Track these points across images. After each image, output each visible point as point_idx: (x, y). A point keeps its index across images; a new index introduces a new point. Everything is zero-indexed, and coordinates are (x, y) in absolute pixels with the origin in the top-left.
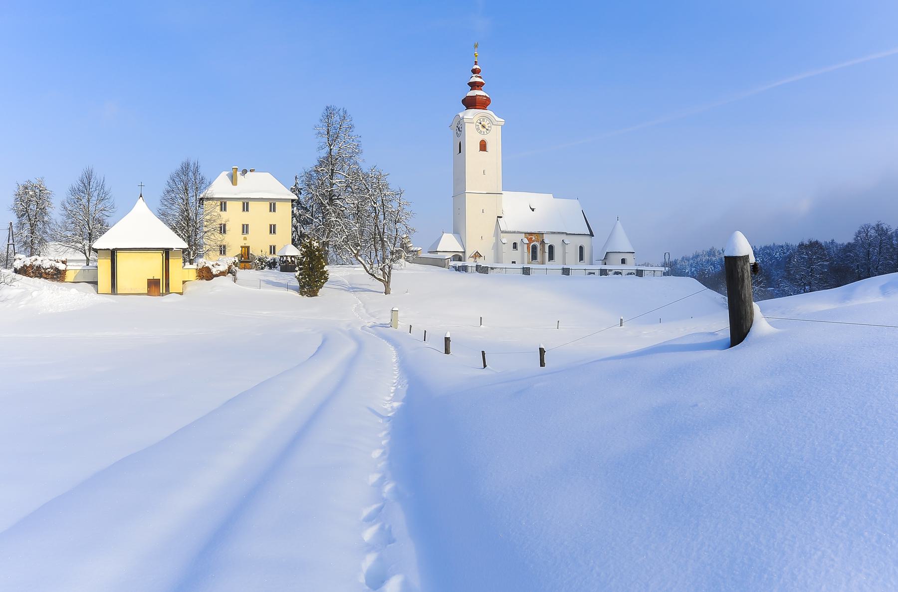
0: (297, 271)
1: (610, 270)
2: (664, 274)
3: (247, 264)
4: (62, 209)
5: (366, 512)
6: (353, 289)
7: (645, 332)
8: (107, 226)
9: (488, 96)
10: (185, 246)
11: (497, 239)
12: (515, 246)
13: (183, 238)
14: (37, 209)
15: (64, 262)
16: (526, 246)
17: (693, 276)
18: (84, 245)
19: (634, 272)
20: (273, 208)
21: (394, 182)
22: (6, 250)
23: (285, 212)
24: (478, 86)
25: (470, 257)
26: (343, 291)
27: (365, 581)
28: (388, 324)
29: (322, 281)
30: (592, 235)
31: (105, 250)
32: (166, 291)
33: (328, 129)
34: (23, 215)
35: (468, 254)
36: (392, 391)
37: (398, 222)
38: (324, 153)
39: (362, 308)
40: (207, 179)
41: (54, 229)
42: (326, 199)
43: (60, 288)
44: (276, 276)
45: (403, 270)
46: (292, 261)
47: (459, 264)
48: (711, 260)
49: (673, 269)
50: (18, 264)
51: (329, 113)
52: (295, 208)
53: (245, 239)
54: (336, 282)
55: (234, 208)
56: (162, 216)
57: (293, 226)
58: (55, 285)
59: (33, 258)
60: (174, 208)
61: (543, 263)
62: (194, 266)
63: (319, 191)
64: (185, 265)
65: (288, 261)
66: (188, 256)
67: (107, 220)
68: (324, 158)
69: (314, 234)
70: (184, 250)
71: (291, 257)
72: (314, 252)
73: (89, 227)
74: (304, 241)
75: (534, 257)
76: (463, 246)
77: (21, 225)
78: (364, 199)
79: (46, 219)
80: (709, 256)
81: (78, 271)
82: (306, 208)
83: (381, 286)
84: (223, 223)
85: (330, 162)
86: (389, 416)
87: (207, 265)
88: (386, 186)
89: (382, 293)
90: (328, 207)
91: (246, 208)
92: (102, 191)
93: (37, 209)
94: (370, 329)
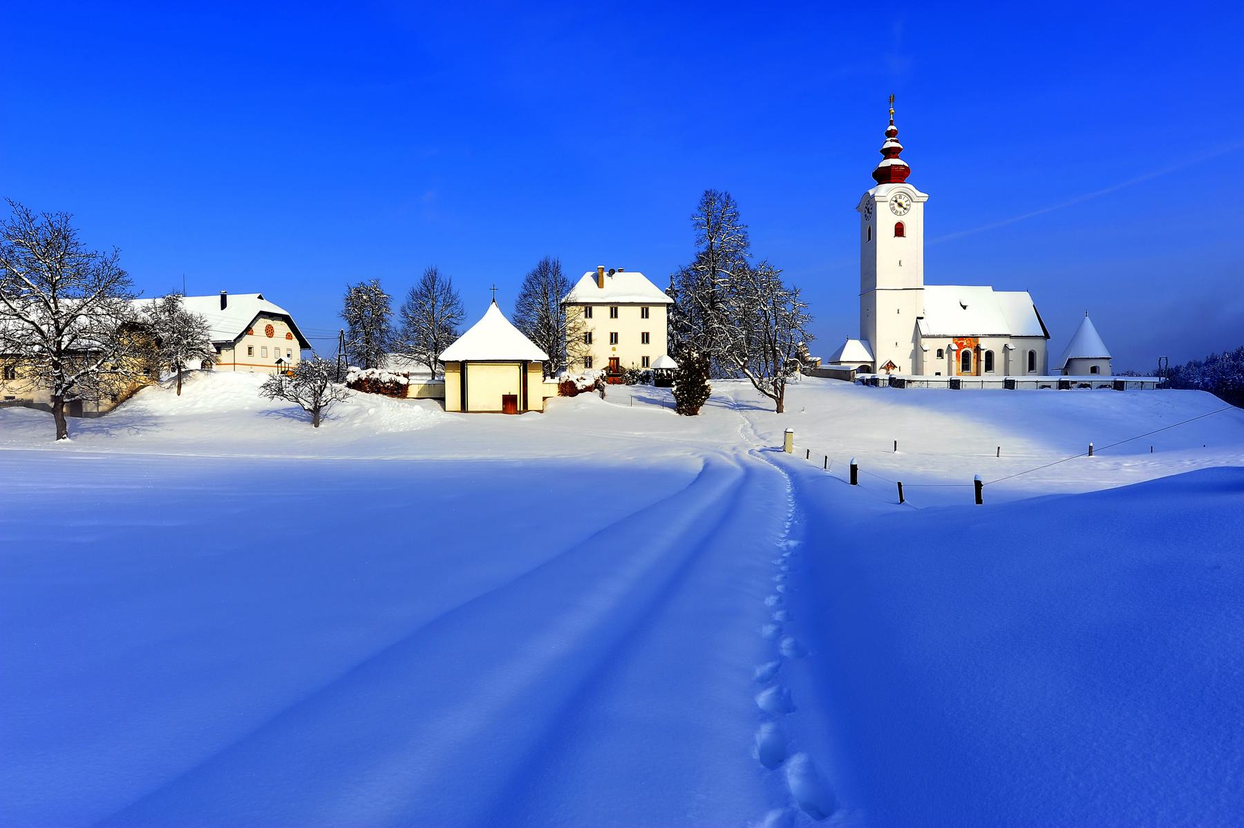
0: (673, 386)
1: (1073, 382)
2: (1159, 386)
3: (616, 378)
4: (402, 316)
5: (760, 671)
6: (739, 406)
7: (1127, 465)
8: (455, 335)
9: (906, 165)
10: (546, 357)
11: (916, 346)
12: (940, 353)
13: (543, 349)
14: (372, 315)
15: (405, 376)
16: (954, 353)
17: (1205, 388)
18: (429, 357)
19: (1110, 384)
20: (645, 314)
21: (788, 279)
22: (337, 361)
23: (659, 317)
24: (894, 153)
25: (881, 368)
26: (727, 409)
27: (759, 757)
28: (780, 448)
29: (703, 397)
30: (1047, 336)
31: (453, 362)
32: (524, 408)
33: (708, 219)
34: (356, 323)
35: (878, 365)
36: (787, 527)
37: (793, 328)
38: (703, 248)
39: (750, 429)
40: (570, 279)
41: (394, 338)
42: (707, 303)
43: (401, 405)
44: (649, 391)
45: (799, 386)
46: (668, 374)
47: (868, 376)
48: (1238, 365)
49: (1174, 379)
50: (351, 378)
51: (709, 198)
52: (671, 314)
53: (614, 349)
54: (719, 399)
55: (601, 313)
56: (518, 324)
57: (669, 334)
58: (396, 402)
59: (370, 371)
60: (532, 314)
61: (978, 374)
62: (556, 380)
63: (698, 293)
64: (545, 379)
65: (664, 375)
66: (550, 368)
67: (456, 328)
68: (704, 254)
69: (693, 344)
70: (545, 362)
71: (667, 370)
72: (694, 364)
73: (434, 336)
74: (682, 351)
75: (966, 366)
76: (873, 354)
77: (354, 334)
78: (752, 302)
79: (383, 327)
80: (1233, 360)
81: (422, 386)
82: (684, 313)
83: (773, 404)
84: (589, 331)
85: (709, 257)
86: (784, 557)
87: (570, 379)
88: (779, 285)
89: (774, 411)
90: (709, 312)
91: (614, 314)
92: (449, 295)
93: (372, 315)
94: (759, 453)
